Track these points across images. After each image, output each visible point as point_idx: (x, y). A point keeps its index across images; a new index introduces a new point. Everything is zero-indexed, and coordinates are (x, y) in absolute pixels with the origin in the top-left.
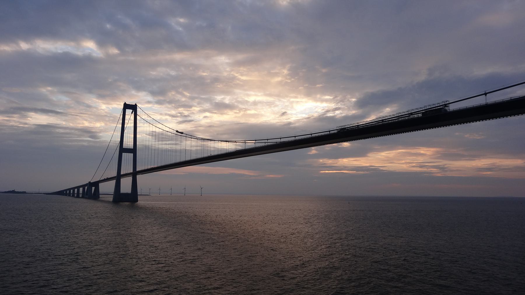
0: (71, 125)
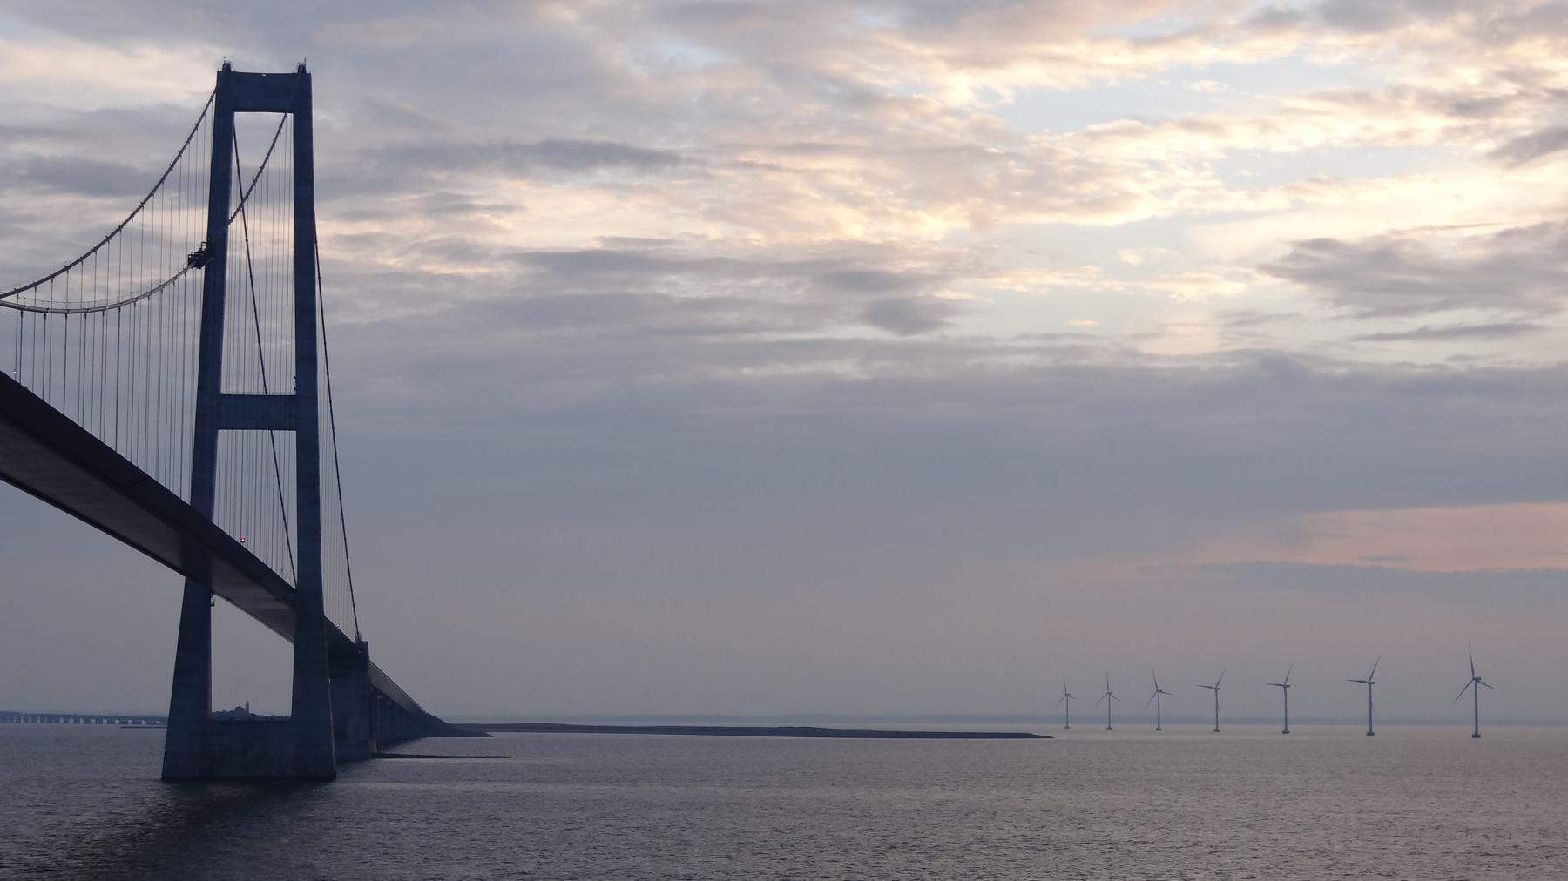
0: (757, 238)
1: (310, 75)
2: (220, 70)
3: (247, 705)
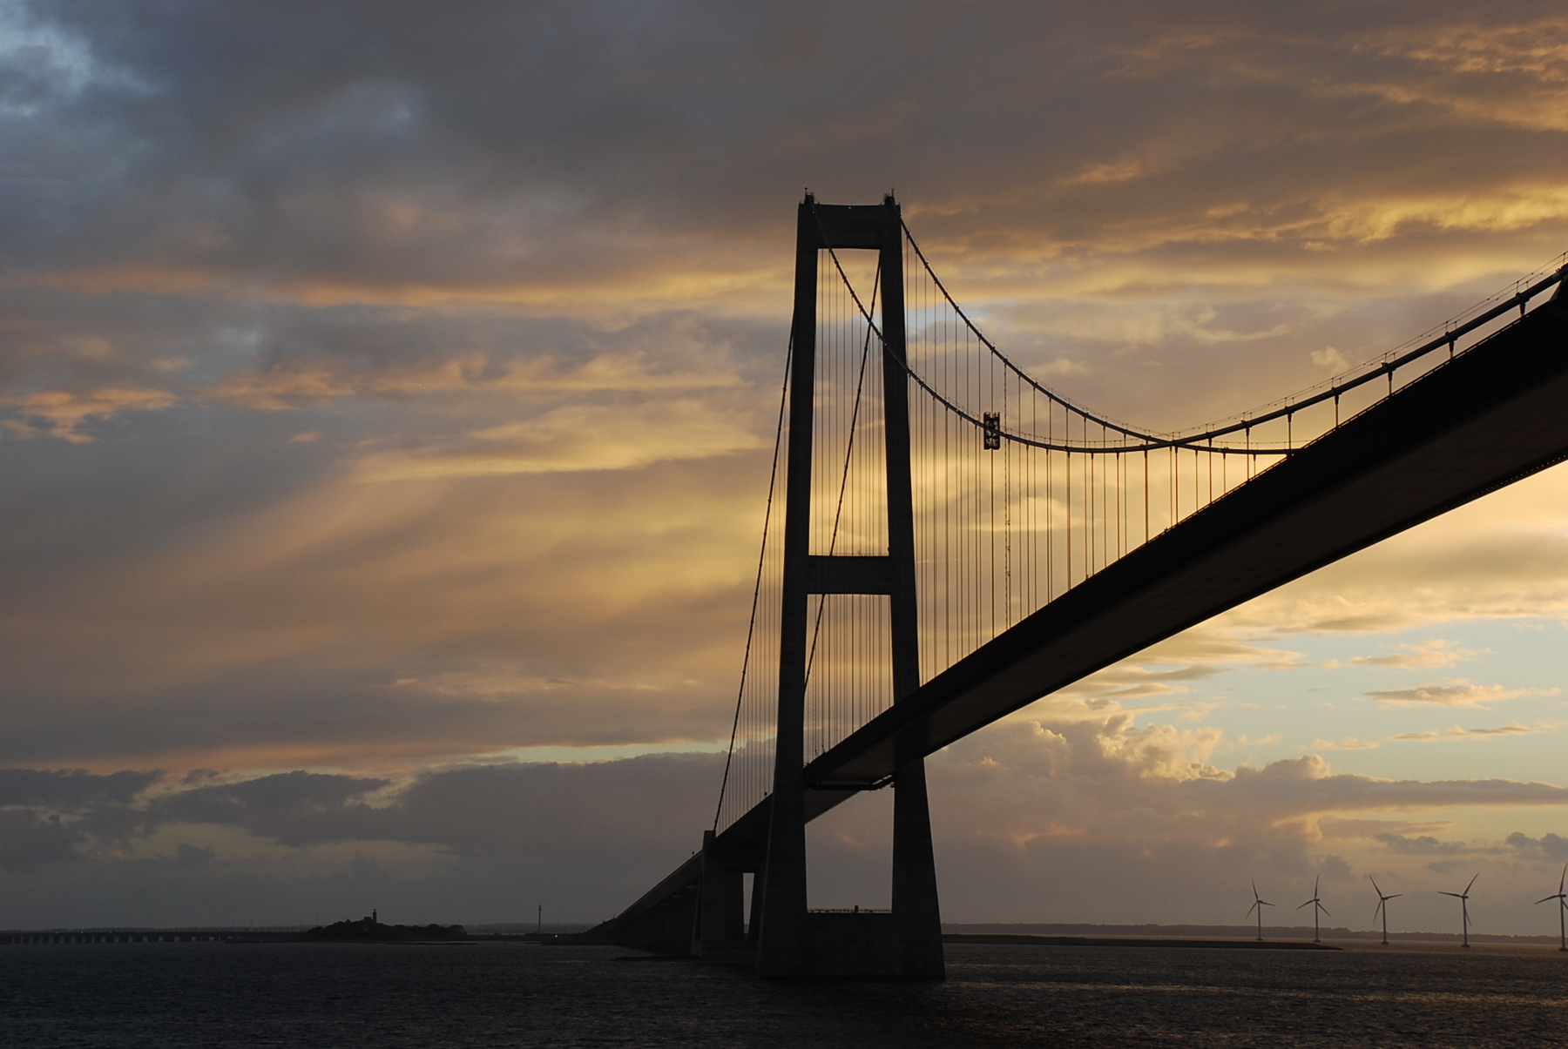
1: (899, 207)
2: (803, 203)
3: (375, 914)
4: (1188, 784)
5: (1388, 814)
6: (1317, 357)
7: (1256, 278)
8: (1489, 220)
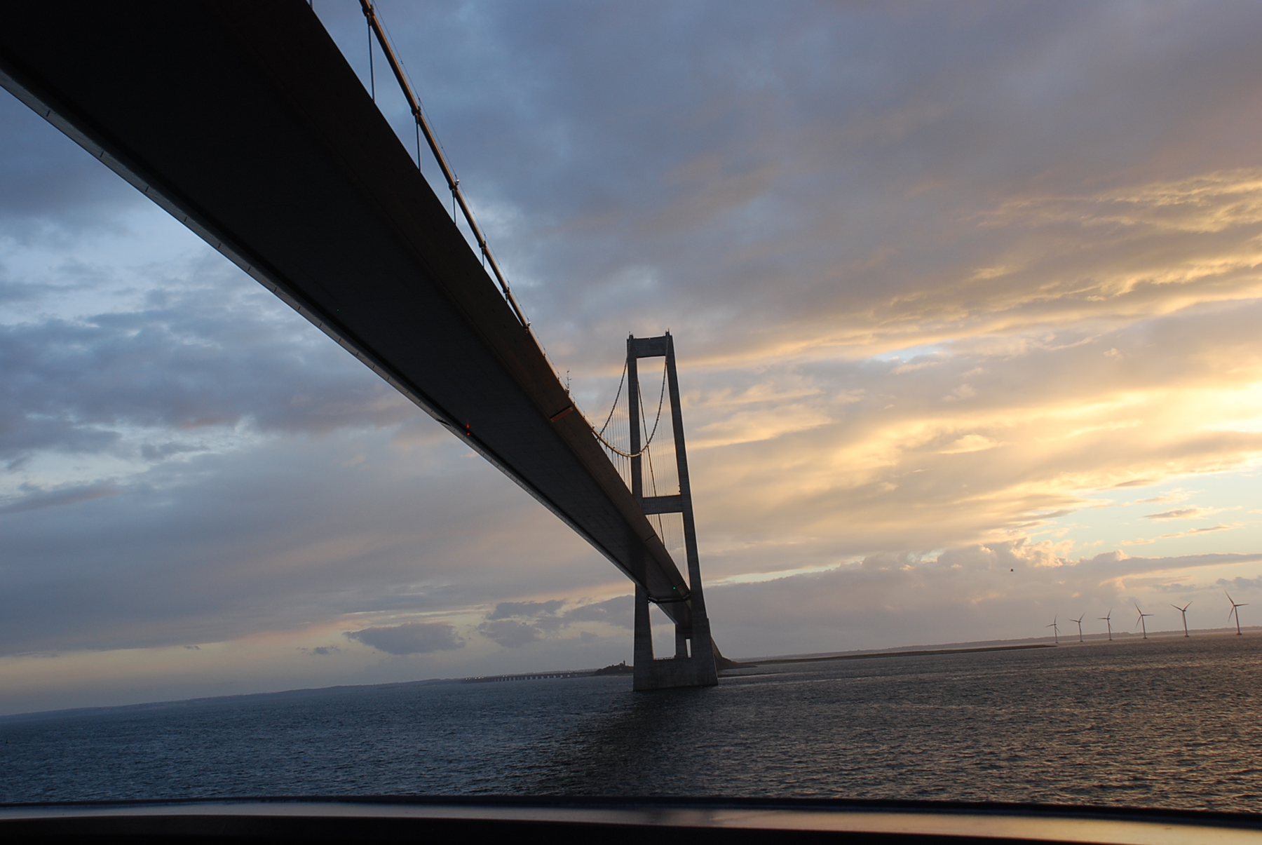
4: (1057, 569)
5: (1158, 574)
6: (1106, 353)
7: (1072, 317)
8: (1180, 278)
